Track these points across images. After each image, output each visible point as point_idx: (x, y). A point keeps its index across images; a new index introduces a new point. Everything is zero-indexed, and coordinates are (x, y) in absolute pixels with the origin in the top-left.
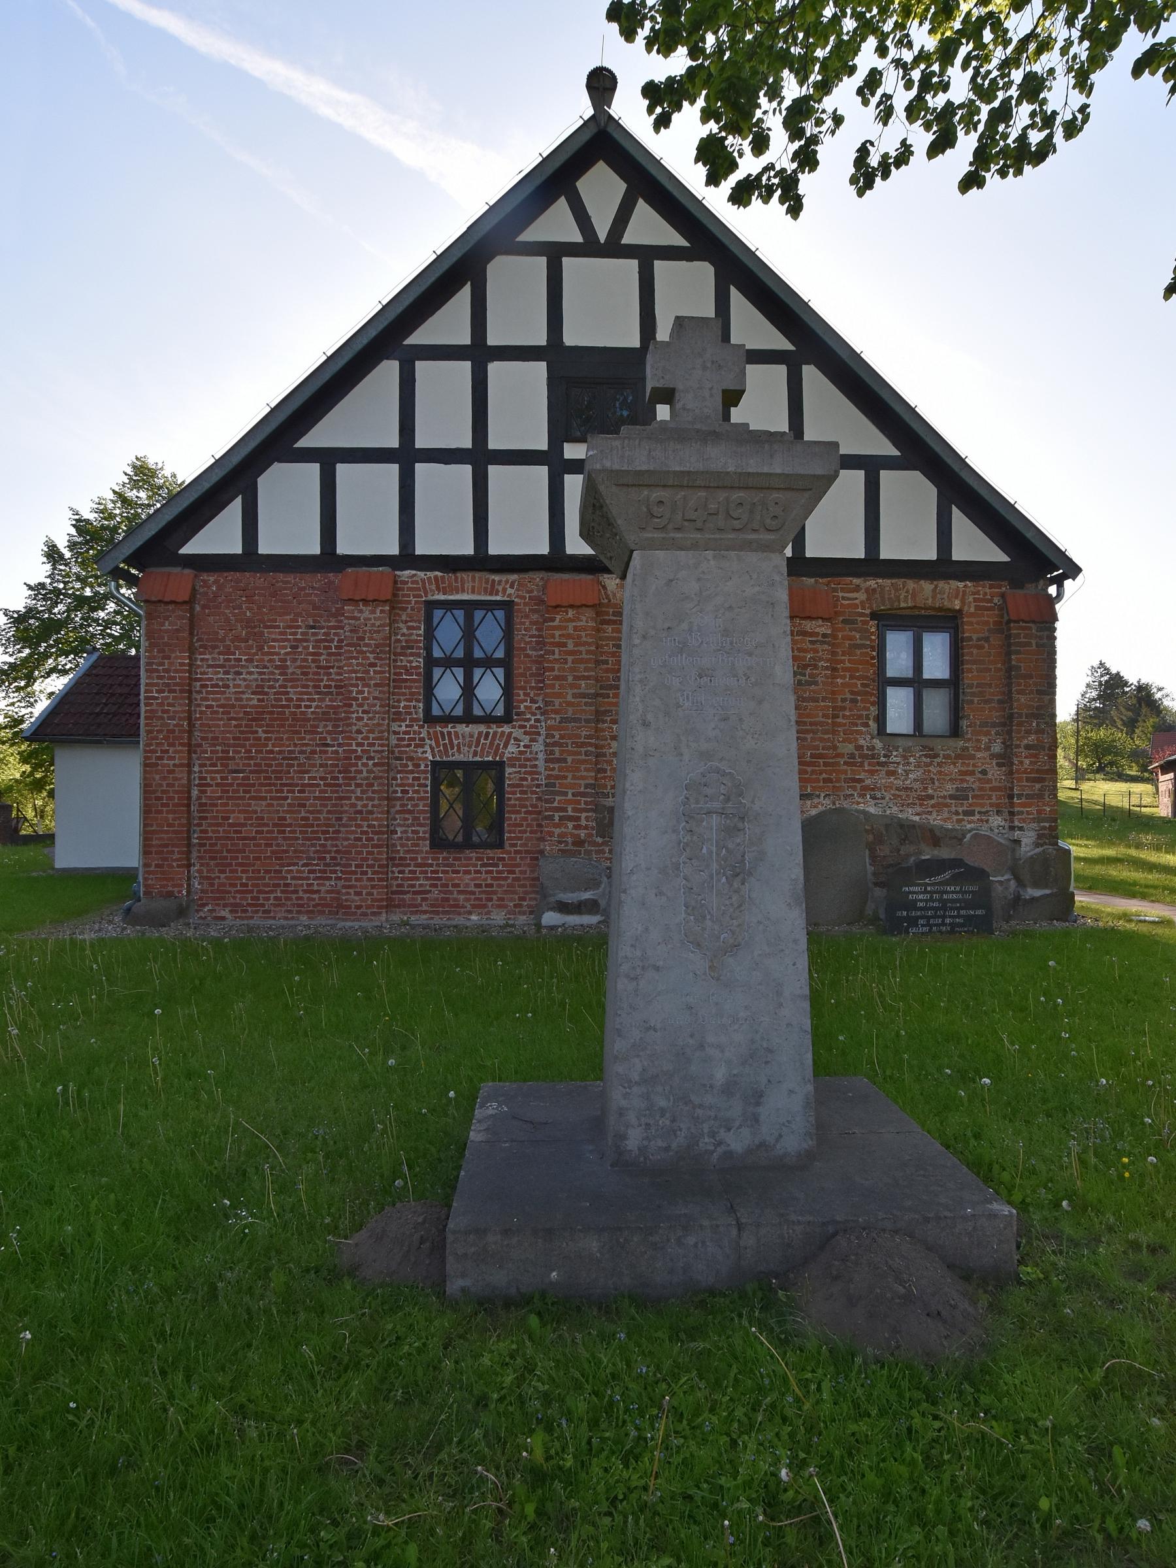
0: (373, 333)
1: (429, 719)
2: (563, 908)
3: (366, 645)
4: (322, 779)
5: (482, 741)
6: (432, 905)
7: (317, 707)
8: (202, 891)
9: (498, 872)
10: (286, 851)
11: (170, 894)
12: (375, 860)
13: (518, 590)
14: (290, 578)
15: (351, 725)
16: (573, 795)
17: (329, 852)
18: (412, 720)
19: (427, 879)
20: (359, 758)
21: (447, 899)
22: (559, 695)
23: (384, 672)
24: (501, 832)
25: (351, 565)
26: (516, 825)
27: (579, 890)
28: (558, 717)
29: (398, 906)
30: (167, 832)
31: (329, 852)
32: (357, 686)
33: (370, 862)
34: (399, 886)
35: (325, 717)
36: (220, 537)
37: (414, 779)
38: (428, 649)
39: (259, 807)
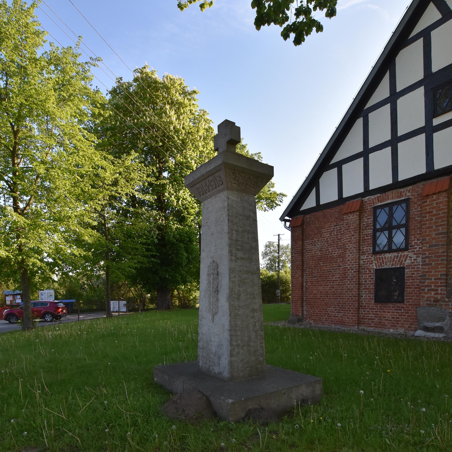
0: (351, 111)
1: (375, 253)
2: (426, 329)
3: (351, 229)
4: (339, 278)
5: (395, 259)
6: (375, 324)
7: (337, 253)
8: (307, 315)
9: (401, 313)
10: (328, 303)
11: (297, 315)
12: (354, 306)
13: (412, 193)
14: (329, 211)
15: (346, 258)
16: (435, 279)
17: (341, 303)
18: (368, 254)
19: (373, 314)
20: (349, 270)
21: (381, 322)
22: (429, 235)
23: (357, 238)
24: (403, 297)
25: (348, 201)
26: (409, 293)
27: (435, 322)
28: (428, 245)
29: (363, 324)
30: (297, 296)
31: (341, 303)
32: (348, 244)
33: (352, 307)
34: (363, 316)
35: (340, 256)
36: (310, 203)
37: (369, 276)
38: (375, 226)
39: (321, 288)
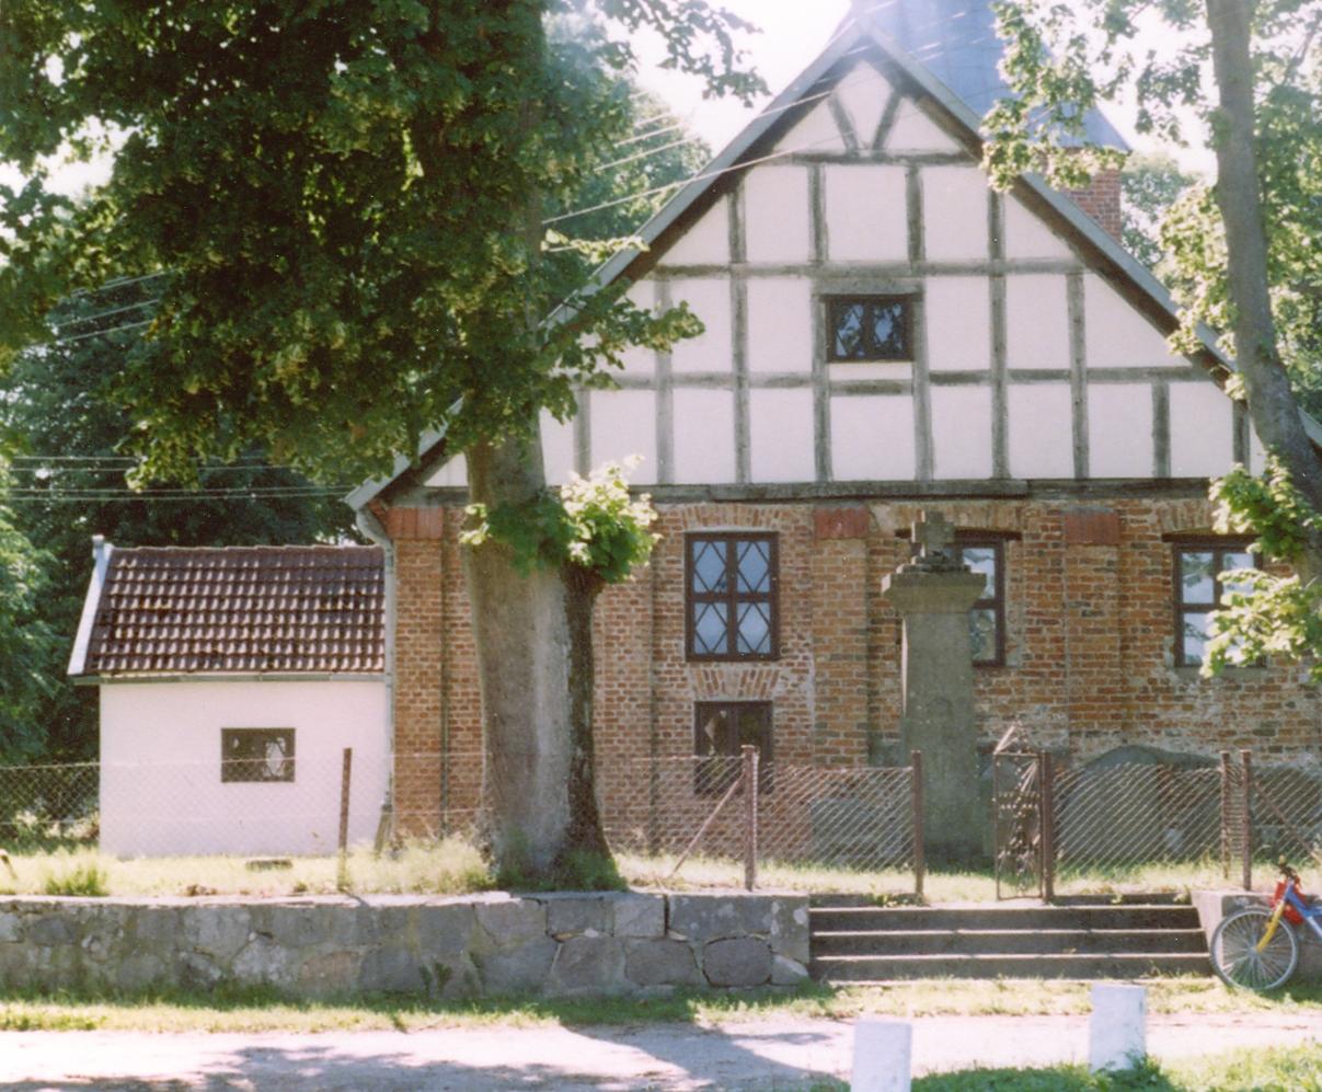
18: (674, 659)
20: (621, 699)
28: (828, 654)
32: (617, 624)
